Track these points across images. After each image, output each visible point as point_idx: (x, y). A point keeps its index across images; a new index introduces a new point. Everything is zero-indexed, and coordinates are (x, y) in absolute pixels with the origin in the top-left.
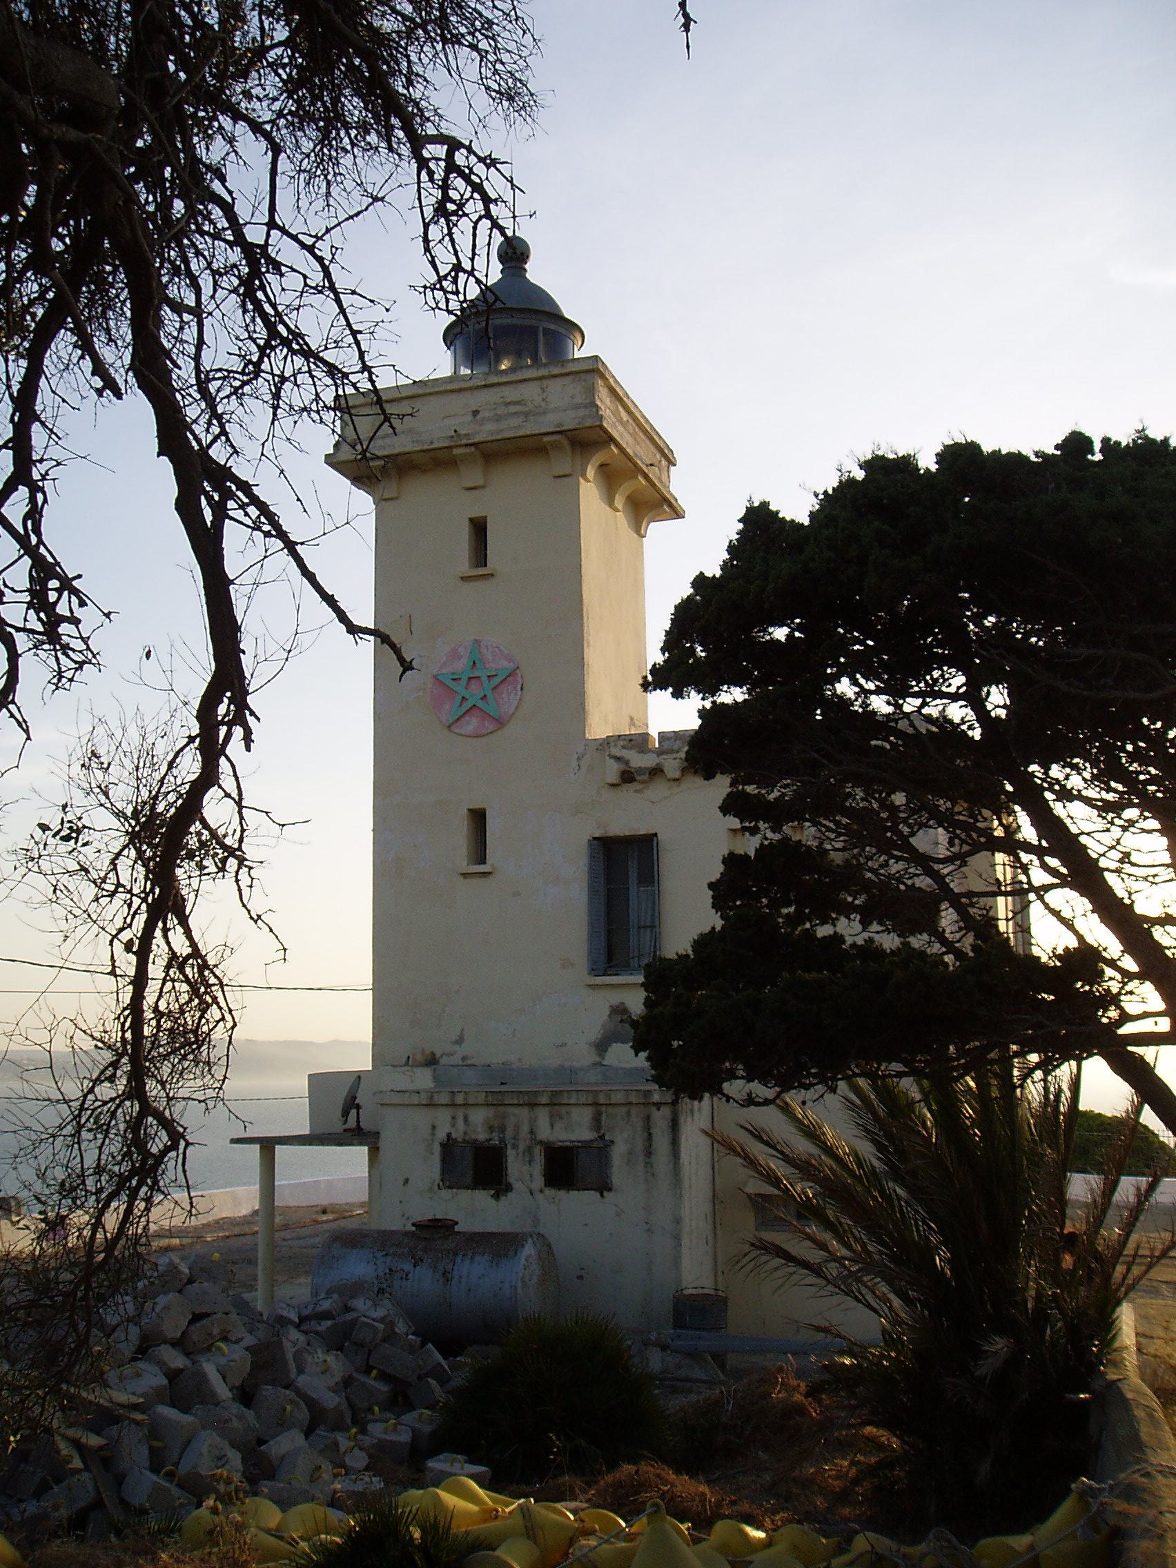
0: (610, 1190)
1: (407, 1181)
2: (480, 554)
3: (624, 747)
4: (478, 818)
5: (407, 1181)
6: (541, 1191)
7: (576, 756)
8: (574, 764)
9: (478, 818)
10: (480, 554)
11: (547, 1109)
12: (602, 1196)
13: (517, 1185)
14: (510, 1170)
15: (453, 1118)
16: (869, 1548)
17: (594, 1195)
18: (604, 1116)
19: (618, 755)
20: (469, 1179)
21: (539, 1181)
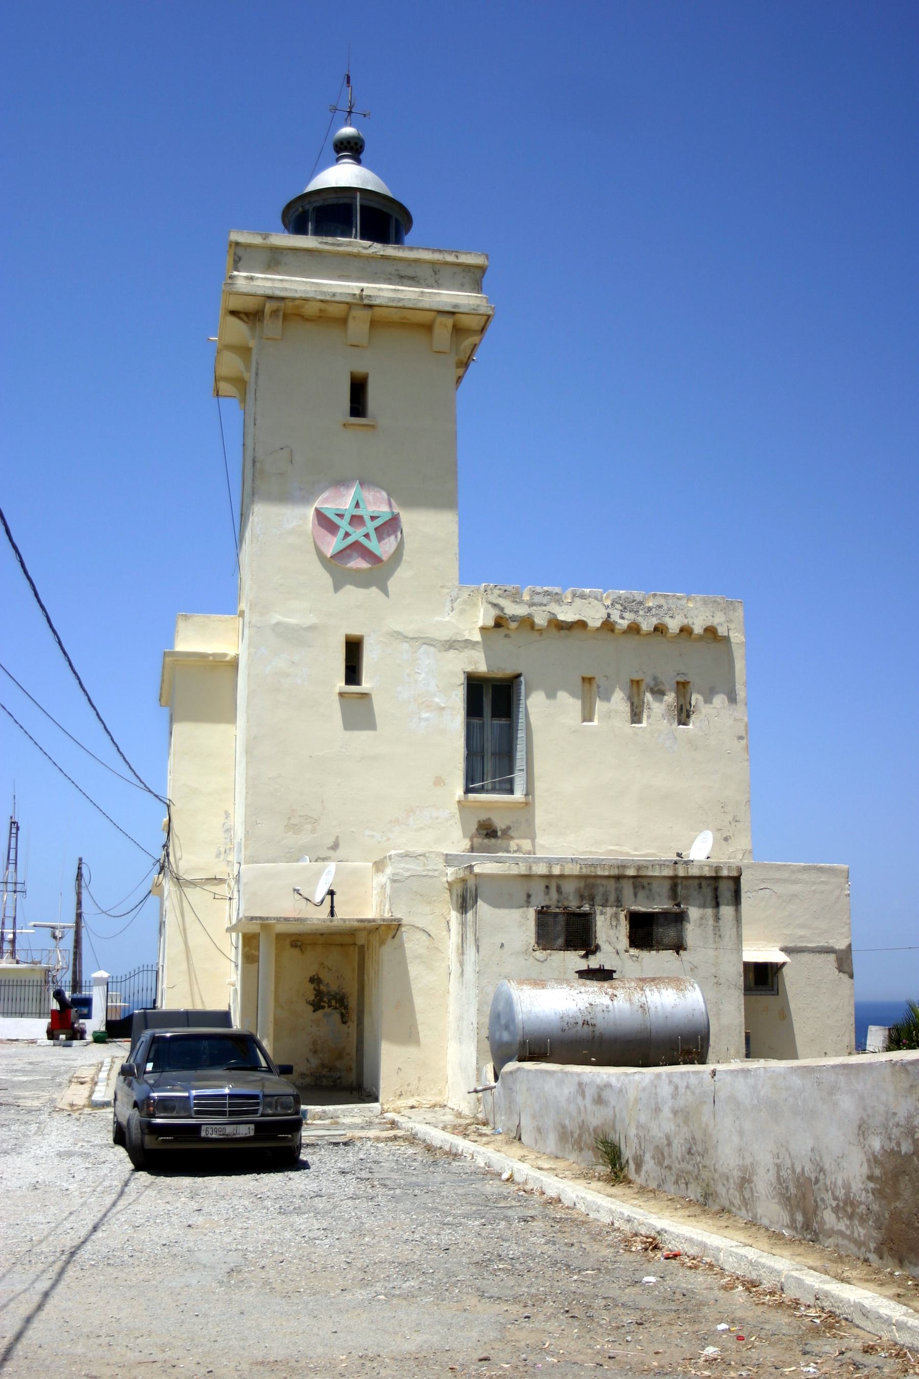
0: (685, 949)
1: (502, 945)
2: (348, 82)
3: (499, 596)
4: (354, 649)
5: (502, 945)
6: (627, 951)
7: (449, 599)
8: (448, 605)
9: (354, 649)
10: (348, 82)
11: (631, 881)
12: (678, 953)
13: (604, 946)
14: (598, 935)
15: (547, 887)
16: (185, 889)
17: (669, 954)
18: (679, 888)
19: (495, 601)
20: (560, 941)
21: (624, 942)
